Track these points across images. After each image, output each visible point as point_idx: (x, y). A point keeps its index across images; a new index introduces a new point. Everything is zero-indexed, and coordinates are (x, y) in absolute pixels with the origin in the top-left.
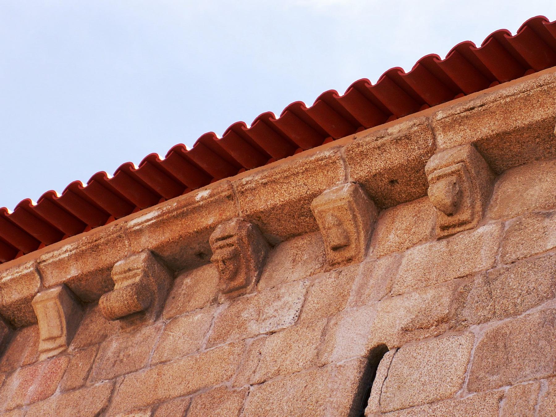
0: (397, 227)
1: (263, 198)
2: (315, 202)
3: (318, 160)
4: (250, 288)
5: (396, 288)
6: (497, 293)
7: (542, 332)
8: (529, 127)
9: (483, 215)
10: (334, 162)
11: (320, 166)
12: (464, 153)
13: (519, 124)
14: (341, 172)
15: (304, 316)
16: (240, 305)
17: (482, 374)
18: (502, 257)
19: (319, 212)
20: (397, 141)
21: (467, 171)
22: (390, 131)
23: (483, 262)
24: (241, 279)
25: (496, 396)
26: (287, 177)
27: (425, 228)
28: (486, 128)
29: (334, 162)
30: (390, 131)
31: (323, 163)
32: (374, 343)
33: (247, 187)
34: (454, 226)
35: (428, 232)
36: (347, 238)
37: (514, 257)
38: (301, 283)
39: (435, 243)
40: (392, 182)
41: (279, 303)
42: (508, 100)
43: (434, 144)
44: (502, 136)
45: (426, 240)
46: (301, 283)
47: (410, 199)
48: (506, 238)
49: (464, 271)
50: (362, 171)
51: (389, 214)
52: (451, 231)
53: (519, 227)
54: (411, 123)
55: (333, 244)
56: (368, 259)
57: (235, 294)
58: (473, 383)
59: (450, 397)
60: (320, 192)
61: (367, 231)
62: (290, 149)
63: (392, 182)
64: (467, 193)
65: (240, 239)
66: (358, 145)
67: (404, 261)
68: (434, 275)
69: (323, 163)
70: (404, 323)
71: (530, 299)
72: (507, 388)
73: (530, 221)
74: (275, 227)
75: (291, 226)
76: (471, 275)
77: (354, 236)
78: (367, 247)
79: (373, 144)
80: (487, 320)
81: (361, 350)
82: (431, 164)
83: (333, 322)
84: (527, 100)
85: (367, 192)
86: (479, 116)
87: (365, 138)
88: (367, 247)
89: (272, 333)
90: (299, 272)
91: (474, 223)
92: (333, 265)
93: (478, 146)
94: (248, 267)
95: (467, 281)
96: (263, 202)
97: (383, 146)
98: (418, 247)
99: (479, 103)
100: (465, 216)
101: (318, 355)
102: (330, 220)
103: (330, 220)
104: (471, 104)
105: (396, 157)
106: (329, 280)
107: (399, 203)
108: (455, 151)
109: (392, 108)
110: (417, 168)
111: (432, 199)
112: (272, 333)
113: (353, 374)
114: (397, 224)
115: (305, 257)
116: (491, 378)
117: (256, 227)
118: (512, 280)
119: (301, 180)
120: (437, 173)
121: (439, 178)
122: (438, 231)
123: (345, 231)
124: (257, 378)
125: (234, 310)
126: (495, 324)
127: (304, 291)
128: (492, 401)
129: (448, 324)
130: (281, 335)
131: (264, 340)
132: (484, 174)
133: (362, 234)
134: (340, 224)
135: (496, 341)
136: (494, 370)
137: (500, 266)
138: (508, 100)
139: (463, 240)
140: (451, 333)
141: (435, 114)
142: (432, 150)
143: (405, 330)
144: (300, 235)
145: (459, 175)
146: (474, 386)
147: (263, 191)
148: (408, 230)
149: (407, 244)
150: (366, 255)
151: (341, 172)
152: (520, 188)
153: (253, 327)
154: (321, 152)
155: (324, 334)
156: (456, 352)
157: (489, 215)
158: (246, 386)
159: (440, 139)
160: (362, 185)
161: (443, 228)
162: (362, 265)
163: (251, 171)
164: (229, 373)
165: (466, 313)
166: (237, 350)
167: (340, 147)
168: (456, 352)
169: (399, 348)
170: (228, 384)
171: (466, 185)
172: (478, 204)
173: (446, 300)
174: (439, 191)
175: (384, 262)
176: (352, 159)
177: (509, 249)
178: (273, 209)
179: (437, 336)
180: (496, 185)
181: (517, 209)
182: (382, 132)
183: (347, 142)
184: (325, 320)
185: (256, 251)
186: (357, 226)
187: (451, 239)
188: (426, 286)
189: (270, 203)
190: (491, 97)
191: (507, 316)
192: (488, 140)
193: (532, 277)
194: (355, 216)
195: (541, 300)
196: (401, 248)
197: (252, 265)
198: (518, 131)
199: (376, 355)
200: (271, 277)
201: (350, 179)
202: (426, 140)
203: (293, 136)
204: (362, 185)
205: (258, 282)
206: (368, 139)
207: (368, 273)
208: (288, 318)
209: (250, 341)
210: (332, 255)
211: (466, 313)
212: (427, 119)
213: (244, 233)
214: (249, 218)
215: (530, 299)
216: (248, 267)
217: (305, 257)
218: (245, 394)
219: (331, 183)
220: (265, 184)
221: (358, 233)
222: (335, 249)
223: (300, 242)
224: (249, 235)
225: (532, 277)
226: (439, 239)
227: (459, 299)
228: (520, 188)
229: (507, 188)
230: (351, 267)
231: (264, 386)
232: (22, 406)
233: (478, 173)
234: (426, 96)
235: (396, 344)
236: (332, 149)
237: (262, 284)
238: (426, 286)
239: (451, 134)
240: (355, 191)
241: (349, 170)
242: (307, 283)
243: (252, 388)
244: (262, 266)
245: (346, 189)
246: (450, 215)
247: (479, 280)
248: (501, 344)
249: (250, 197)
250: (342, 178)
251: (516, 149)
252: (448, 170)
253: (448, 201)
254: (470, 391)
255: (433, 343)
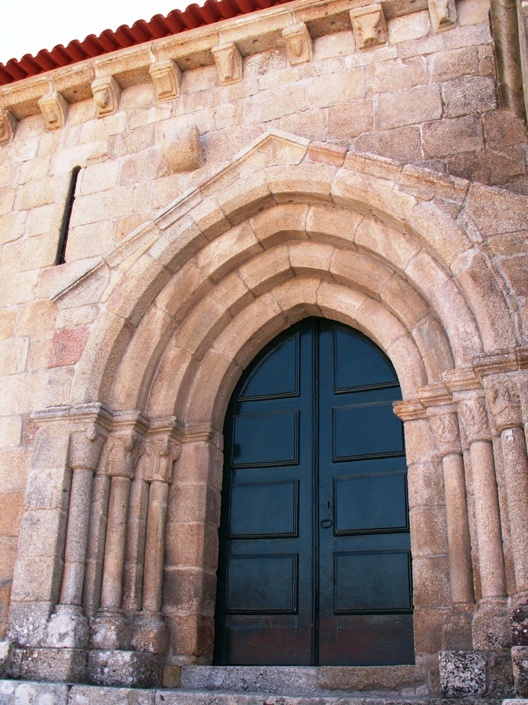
0: (80, 111)
1: (14, 99)
2: (40, 101)
3: (39, 81)
4: (10, 141)
5: (81, 141)
6: (128, 143)
7: (150, 160)
8: (137, 69)
9: (118, 108)
10: (47, 82)
11: (41, 84)
12: (109, 80)
13: (133, 67)
14: (51, 87)
15: (39, 153)
16: (7, 148)
17: (125, 178)
18: (129, 126)
19: (42, 106)
20: (77, 73)
21: (111, 88)
22: (73, 68)
23: (120, 129)
24: (6, 137)
25: (133, 187)
26: (24, 89)
27: (92, 113)
28: (118, 69)
29: (47, 82)
30: (73, 68)
31: (42, 82)
32: (74, 166)
33: (5, 93)
34: (105, 113)
35: (93, 115)
36: (56, 118)
37: (134, 127)
38: (35, 138)
39: (97, 120)
40: (75, 92)
41: (25, 148)
42: (128, 56)
43: (94, 75)
44: (125, 73)
45: (93, 119)
46: (35, 138)
47: (83, 99)
48: (130, 119)
49: (112, 133)
50: (62, 87)
51: (74, 107)
52: (104, 115)
53: (135, 113)
54: (83, 65)
55: (50, 120)
56: (66, 127)
57: (3, 143)
58: (122, 182)
59: (112, 188)
60: (42, 96)
61: (64, 115)
62: (24, 75)
63: (75, 92)
64: (111, 98)
65: (4, 118)
66: (59, 75)
67: (84, 128)
68: (98, 135)
69: (42, 82)
70: (88, 156)
71: (143, 146)
72: (137, 184)
73: (139, 111)
74: (19, 112)
75: (27, 112)
76: (115, 135)
77: (59, 117)
78: (65, 122)
79: (65, 75)
80: (125, 155)
81: (70, 169)
82: (93, 86)
83: (53, 156)
84: (136, 57)
85: (63, 96)
86: (114, 63)
87: (62, 71)
88: (65, 122)
89: (25, 161)
90: (34, 133)
91: (115, 111)
92: (50, 130)
93: (115, 77)
94: (9, 131)
95: (114, 138)
96: (14, 100)
97: (71, 75)
98: (89, 122)
99: (114, 57)
100: (110, 108)
101: (49, 171)
102: (48, 109)
103: (48, 109)
104: (111, 58)
105: (77, 81)
106: (49, 137)
107: (78, 101)
108: (104, 79)
109: (73, 58)
110: (88, 85)
111: (96, 101)
112: (25, 161)
113: (67, 180)
114: (78, 111)
115: (36, 126)
116: (129, 180)
117: (10, 112)
118: (134, 137)
119: (31, 90)
120: (97, 89)
121: (98, 91)
122: (98, 115)
123: (55, 114)
124: (21, 182)
125: (4, 151)
126: (128, 157)
127: (38, 142)
128: (131, 189)
129: (107, 156)
130: (29, 162)
131: (21, 165)
132: (118, 89)
133: (63, 116)
134: (52, 111)
135: (130, 164)
136: (130, 176)
137: (128, 131)
138: (128, 56)
139: (110, 119)
140: (109, 160)
141: (94, 61)
142: (93, 78)
143: (89, 159)
144: (31, 115)
145: (107, 91)
146: (123, 183)
147: (13, 95)
148: (83, 114)
149: (84, 120)
150: (65, 125)
151: (51, 87)
152: (134, 96)
153: (15, 159)
154: (41, 77)
155: (50, 161)
156: (113, 169)
157: (121, 108)
158: (17, 186)
159: (97, 73)
160: (61, 93)
161: (101, 113)
162: (64, 130)
163: (6, 85)
164: (7, 180)
165: (115, 152)
166: (9, 169)
167: (49, 75)
168: (113, 169)
169: (86, 168)
170: (7, 185)
171: (110, 94)
172: (116, 103)
173: (106, 146)
174: (99, 97)
175: (75, 129)
176: (56, 81)
177: (131, 123)
178: (19, 104)
179: (103, 162)
180: (122, 94)
181: (133, 105)
182: (70, 69)
183: (52, 72)
184: (50, 156)
185: (12, 123)
186: (60, 112)
187: (104, 118)
188: (96, 140)
189: (17, 101)
190: (120, 55)
191: (134, 153)
192: (119, 74)
193: (143, 136)
194: (59, 108)
195: (148, 146)
196: (82, 123)
197: (11, 130)
198: (132, 70)
199: (76, 171)
200: (20, 135)
201: (55, 91)
202: (90, 74)
203: (26, 69)
204: (61, 93)
205: (14, 137)
206: (63, 72)
207: (67, 134)
208: (32, 155)
209: (15, 165)
210: (49, 125)
211: (115, 152)
212: (91, 64)
213: (6, 115)
214: (7, 108)
215: (143, 146)
216: (9, 131)
217: (36, 126)
218: (16, 190)
219: (46, 92)
220: (14, 92)
221: (61, 115)
222: (51, 123)
223: (32, 119)
224: (8, 116)
225: (143, 136)
226: (99, 118)
227: (111, 145)
228: (134, 96)
229: (128, 95)
230: (58, 130)
231: (25, 185)
232: (460, 268)
233: (115, 89)
234: (89, 53)
235: (85, 166)
236: (46, 76)
237: (16, 139)
238: (96, 140)
239: (102, 71)
240: (59, 96)
241: (55, 86)
242: (39, 138)
243: (19, 187)
244: (15, 130)
245: (54, 95)
246: (104, 108)
247: (119, 137)
248: (132, 165)
249: (7, 98)
250: (51, 90)
251: (132, 78)
252: (102, 88)
253: (103, 102)
254: (121, 185)
255: (102, 165)
